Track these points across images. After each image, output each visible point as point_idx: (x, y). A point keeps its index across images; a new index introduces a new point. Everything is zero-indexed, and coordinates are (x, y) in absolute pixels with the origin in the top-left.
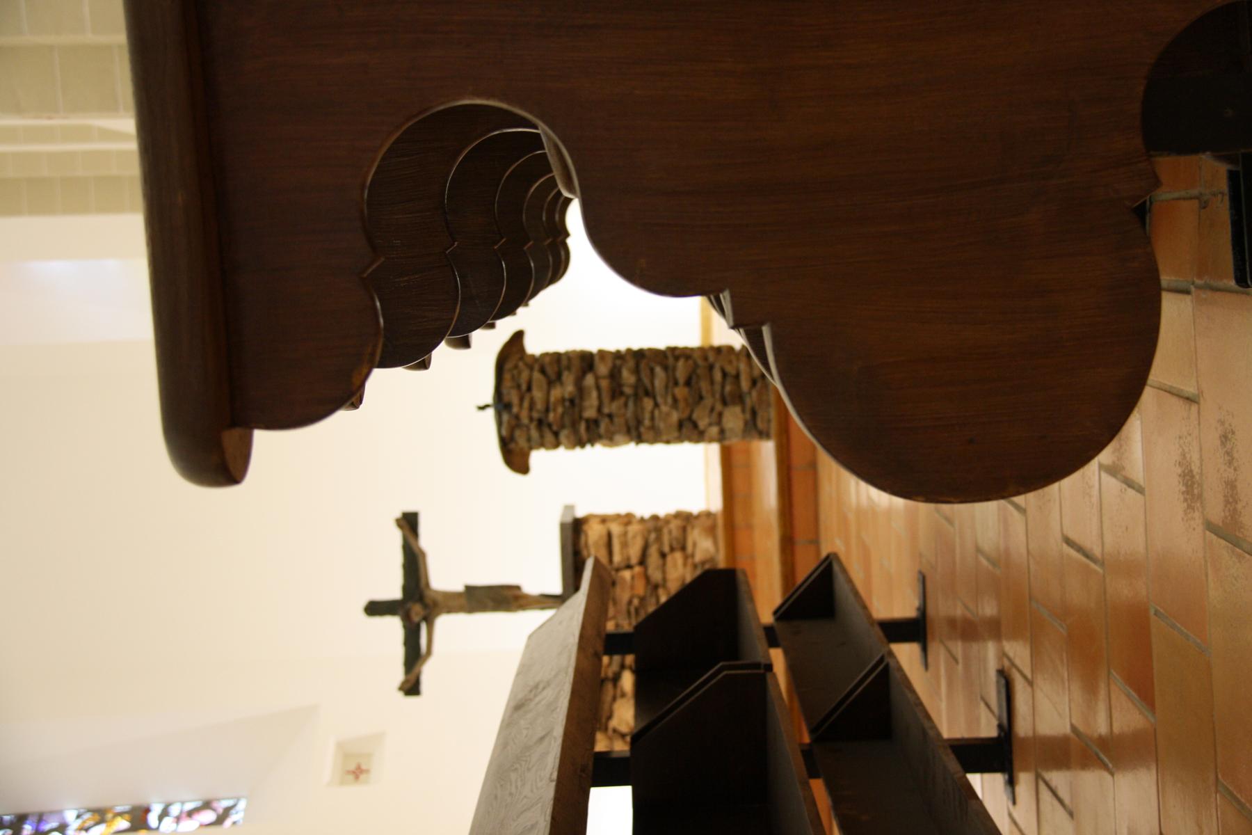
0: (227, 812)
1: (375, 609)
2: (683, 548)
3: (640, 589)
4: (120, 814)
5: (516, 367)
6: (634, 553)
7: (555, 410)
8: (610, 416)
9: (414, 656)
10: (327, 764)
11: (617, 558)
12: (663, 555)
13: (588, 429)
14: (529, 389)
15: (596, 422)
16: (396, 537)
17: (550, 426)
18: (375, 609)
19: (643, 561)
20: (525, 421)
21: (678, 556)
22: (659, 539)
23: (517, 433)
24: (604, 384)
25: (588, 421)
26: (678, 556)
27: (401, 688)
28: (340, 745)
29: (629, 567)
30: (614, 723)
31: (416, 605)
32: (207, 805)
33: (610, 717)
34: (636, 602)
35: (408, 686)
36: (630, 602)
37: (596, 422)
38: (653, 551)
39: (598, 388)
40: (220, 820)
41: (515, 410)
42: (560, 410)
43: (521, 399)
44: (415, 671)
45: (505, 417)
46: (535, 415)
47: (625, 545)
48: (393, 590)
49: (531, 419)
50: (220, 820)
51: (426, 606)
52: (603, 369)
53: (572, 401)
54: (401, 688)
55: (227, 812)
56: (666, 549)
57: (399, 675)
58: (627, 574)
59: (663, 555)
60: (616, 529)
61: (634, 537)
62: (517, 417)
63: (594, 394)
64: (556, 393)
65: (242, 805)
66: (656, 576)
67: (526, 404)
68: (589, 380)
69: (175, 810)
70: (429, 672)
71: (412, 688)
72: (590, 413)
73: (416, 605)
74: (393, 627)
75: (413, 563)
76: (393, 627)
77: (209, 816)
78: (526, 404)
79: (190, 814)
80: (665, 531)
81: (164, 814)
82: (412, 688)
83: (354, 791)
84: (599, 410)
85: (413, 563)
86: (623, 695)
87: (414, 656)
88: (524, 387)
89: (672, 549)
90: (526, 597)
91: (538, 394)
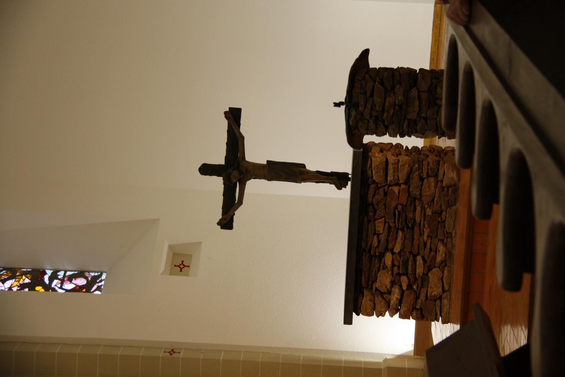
0: (95, 280)
1: (207, 170)
2: (436, 176)
3: (404, 200)
4: (25, 274)
5: (364, 78)
6: (402, 176)
7: (388, 112)
8: (425, 119)
9: (231, 203)
10: (162, 259)
12: (422, 179)
13: (408, 126)
14: (372, 95)
15: (415, 122)
16: (225, 123)
17: (383, 122)
18: (207, 170)
19: (406, 182)
20: (367, 117)
21: (432, 180)
22: (420, 168)
23: (360, 124)
24: (424, 96)
25: (409, 120)
26: (432, 180)
27: (219, 224)
28: (171, 247)
29: (398, 184)
30: (377, 285)
31: (235, 171)
32: (81, 274)
34: (400, 207)
35: (224, 222)
36: (396, 208)
37: (415, 122)
38: (415, 175)
39: (420, 99)
40: (88, 288)
41: (361, 109)
42: (392, 111)
43: (366, 103)
44: (230, 213)
45: (353, 113)
46: (374, 114)
47: (396, 170)
48: (219, 158)
49: (371, 116)
50: (88, 288)
51: (241, 173)
52: (424, 86)
53: (400, 106)
54: (219, 224)
55: (95, 280)
56: (425, 176)
57: (219, 215)
58: (396, 189)
59: (422, 179)
60: (392, 159)
61: (404, 165)
62: (362, 114)
63: (417, 103)
64: (390, 100)
65: (104, 277)
66: (415, 192)
67: (369, 106)
68: (414, 92)
69: (61, 274)
70: (239, 215)
71: (226, 223)
72: (412, 116)
73: (235, 171)
74: (217, 184)
75: (235, 142)
76: (217, 184)
77: (81, 282)
78: (369, 106)
79: (70, 279)
80: (425, 163)
81: (54, 277)
82: (226, 223)
83: (178, 279)
84: (419, 114)
85: (235, 142)
86: (385, 267)
87: (231, 203)
88: (368, 94)
89: (428, 176)
90: (309, 172)
91: (377, 100)
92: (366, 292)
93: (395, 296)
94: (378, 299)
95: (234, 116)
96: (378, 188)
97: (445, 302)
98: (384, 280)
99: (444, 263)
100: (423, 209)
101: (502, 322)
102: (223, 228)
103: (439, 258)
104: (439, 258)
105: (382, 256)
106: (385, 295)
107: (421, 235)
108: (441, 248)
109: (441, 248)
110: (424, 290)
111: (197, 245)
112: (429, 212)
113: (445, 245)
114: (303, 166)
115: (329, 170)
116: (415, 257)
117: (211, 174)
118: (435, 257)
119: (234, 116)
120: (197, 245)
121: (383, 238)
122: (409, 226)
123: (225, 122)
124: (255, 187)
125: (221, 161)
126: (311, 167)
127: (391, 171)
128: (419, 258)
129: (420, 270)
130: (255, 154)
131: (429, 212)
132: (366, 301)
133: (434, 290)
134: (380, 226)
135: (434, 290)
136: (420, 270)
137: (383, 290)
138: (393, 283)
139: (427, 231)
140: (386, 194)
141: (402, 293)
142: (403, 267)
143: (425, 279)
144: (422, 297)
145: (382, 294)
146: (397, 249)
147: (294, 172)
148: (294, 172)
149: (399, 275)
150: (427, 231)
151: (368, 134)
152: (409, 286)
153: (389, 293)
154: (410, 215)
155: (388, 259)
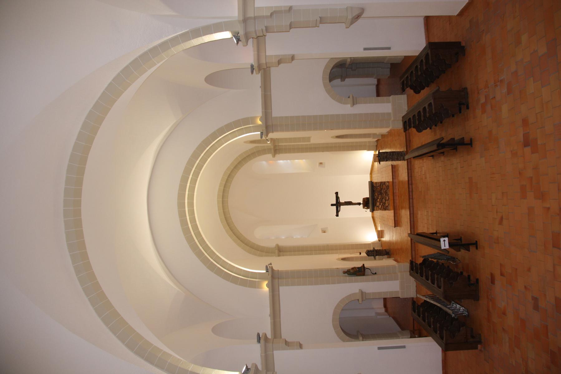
1: (332, 205)
9: (338, 211)
18: (332, 205)
31: (338, 204)
70: (340, 213)
71: (337, 215)
73: (338, 204)
74: (335, 207)
75: (337, 198)
82: (337, 215)
83: (318, 164)
85: (337, 198)
87: (338, 211)
95: (337, 193)
98: (378, 204)
101: (402, 208)
119: (337, 193)
122: (381, 194)
130: (342, 200)
132: (375, 208)
134: (376, 194)
135: (387, 205)
142: (381, 201)
143: (385, 203)
147: (349, 203)
148: (349, 203)
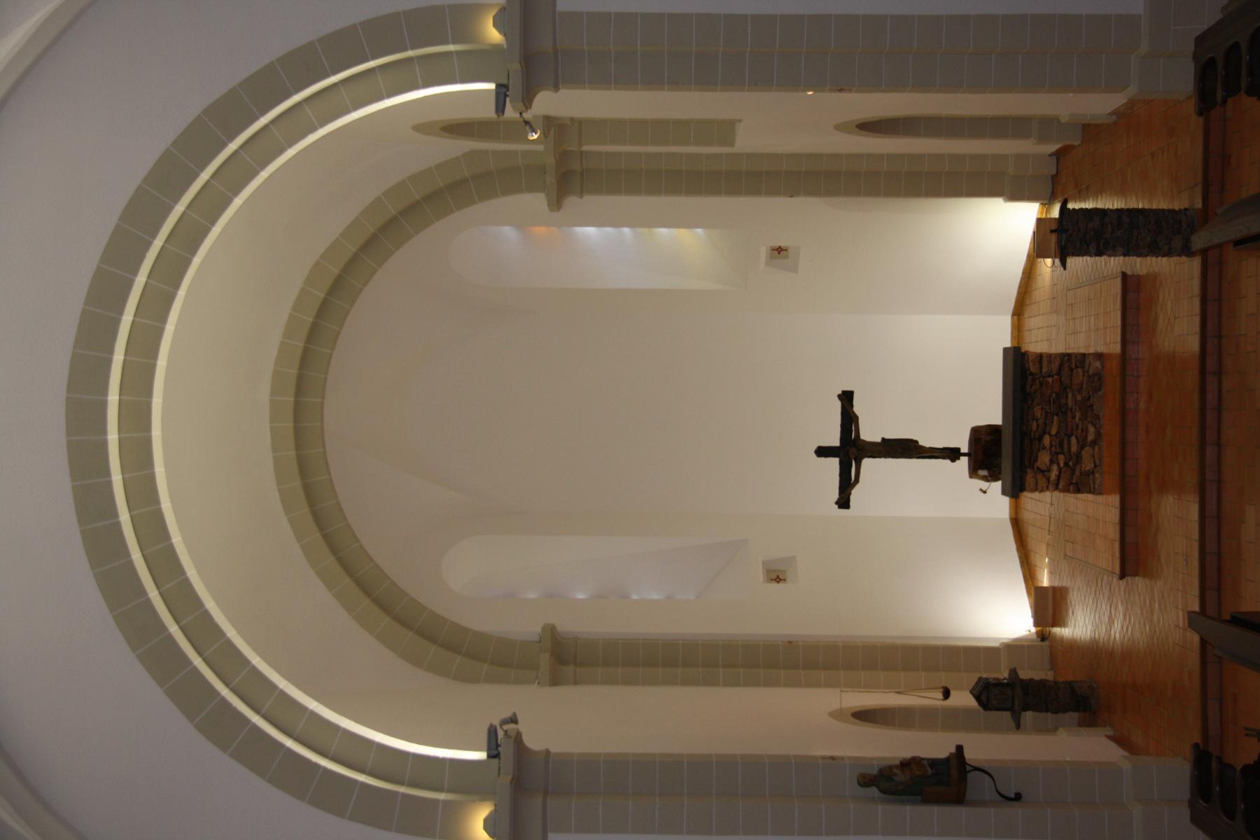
1: (822, 452)
9: (847, 484)
11: (1044, 370)
12: (1072, 370)
16: (838, 405)
18: (822, 452)
21: (1080, 370)
26: (1080, 370)
28: (764, 563)
30: (1038, 464)
31: (851, 450)
33: (1036, 460)
58: (1050, 380)
59: (1072, 370)
70: (856, 495)
71: (844, 503)
73: (851, 450)
74: (832, 465)
75: (849, 420)
76: (834, 463)
82: (844, 503)
85: (849, 420)
86: (1044, 448)
87: (847, 484)
92: (1029, 471)
93: (1054, 474)
94: (1040, 476)
95: (847, 398)
96: (1034, 380)
97: (1097, 475)
98: (1044, 459)
99: (1094, 443)
100: (1074, 395)
102: (840, 507)
103: (1090, 438)
104: (1090, 438)
105: (1040, 439)
106: (1045, 472)
107: (1074, 418)
108: (1091, 429)
109: (1091, 429)
110: (1078, 467)
111: (792, 559)
112: (1079, 398)
113: (1094, 425)
114: (917, 442)
115: (941, 446)
116: (1069, 437)
117: (826, 456)
118: (1086, 437)
119: (847, 398)
120: (792, 559)
121: (1041, 422)
123: (839, 404)
124: (869, 465)
125: (836, 442)
126: (925, 442)
127: (1045, 363)
128: (1073, 440)
129: (1074, 448)
131: (1079, 398)
132: (1029, 479)
133: (1088, 465)
134: (1038, 412)
135: (1088, 465)
136: (1074, 448)
137: (1043, 467)
138: (1052, 462)
139: (1078, 415)
140: (1041, 384)
141: (1060, 470)
143: (1078, 457)
144: (1078, 473)
145: (1043, 472)
146: (1054, 432)
149: (1057, 453)
150: (1078, 415)
151: (1074, 255)
152: (1066, 464)
153: (1049, 471)
154: (1063, 401)
155: (1047, 440)
